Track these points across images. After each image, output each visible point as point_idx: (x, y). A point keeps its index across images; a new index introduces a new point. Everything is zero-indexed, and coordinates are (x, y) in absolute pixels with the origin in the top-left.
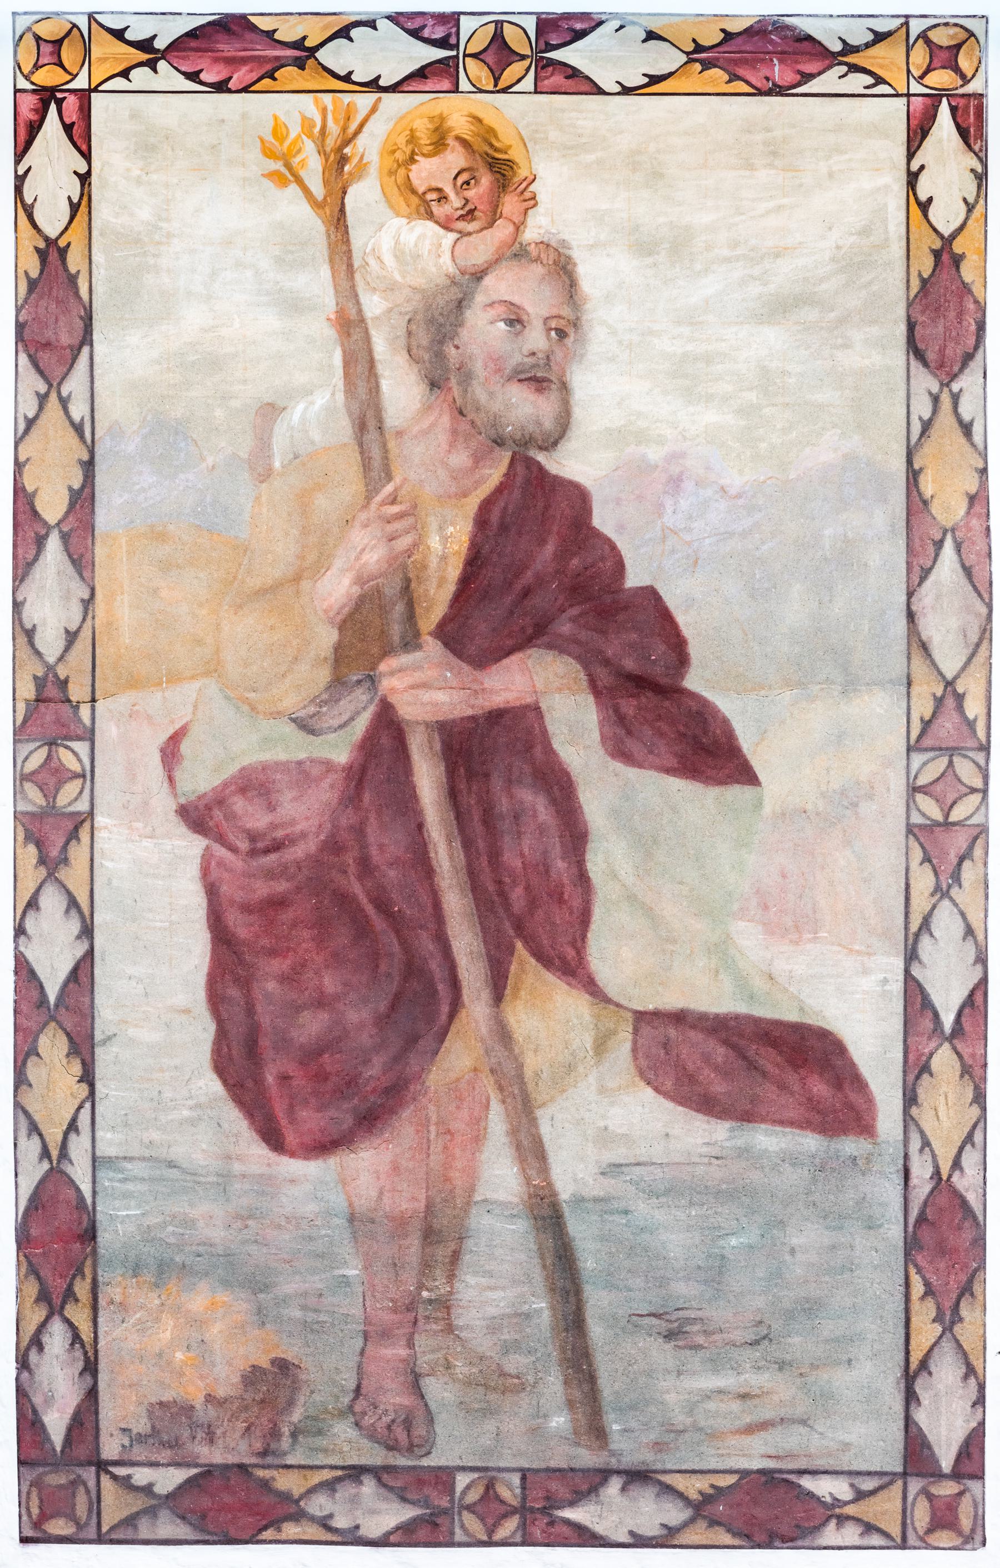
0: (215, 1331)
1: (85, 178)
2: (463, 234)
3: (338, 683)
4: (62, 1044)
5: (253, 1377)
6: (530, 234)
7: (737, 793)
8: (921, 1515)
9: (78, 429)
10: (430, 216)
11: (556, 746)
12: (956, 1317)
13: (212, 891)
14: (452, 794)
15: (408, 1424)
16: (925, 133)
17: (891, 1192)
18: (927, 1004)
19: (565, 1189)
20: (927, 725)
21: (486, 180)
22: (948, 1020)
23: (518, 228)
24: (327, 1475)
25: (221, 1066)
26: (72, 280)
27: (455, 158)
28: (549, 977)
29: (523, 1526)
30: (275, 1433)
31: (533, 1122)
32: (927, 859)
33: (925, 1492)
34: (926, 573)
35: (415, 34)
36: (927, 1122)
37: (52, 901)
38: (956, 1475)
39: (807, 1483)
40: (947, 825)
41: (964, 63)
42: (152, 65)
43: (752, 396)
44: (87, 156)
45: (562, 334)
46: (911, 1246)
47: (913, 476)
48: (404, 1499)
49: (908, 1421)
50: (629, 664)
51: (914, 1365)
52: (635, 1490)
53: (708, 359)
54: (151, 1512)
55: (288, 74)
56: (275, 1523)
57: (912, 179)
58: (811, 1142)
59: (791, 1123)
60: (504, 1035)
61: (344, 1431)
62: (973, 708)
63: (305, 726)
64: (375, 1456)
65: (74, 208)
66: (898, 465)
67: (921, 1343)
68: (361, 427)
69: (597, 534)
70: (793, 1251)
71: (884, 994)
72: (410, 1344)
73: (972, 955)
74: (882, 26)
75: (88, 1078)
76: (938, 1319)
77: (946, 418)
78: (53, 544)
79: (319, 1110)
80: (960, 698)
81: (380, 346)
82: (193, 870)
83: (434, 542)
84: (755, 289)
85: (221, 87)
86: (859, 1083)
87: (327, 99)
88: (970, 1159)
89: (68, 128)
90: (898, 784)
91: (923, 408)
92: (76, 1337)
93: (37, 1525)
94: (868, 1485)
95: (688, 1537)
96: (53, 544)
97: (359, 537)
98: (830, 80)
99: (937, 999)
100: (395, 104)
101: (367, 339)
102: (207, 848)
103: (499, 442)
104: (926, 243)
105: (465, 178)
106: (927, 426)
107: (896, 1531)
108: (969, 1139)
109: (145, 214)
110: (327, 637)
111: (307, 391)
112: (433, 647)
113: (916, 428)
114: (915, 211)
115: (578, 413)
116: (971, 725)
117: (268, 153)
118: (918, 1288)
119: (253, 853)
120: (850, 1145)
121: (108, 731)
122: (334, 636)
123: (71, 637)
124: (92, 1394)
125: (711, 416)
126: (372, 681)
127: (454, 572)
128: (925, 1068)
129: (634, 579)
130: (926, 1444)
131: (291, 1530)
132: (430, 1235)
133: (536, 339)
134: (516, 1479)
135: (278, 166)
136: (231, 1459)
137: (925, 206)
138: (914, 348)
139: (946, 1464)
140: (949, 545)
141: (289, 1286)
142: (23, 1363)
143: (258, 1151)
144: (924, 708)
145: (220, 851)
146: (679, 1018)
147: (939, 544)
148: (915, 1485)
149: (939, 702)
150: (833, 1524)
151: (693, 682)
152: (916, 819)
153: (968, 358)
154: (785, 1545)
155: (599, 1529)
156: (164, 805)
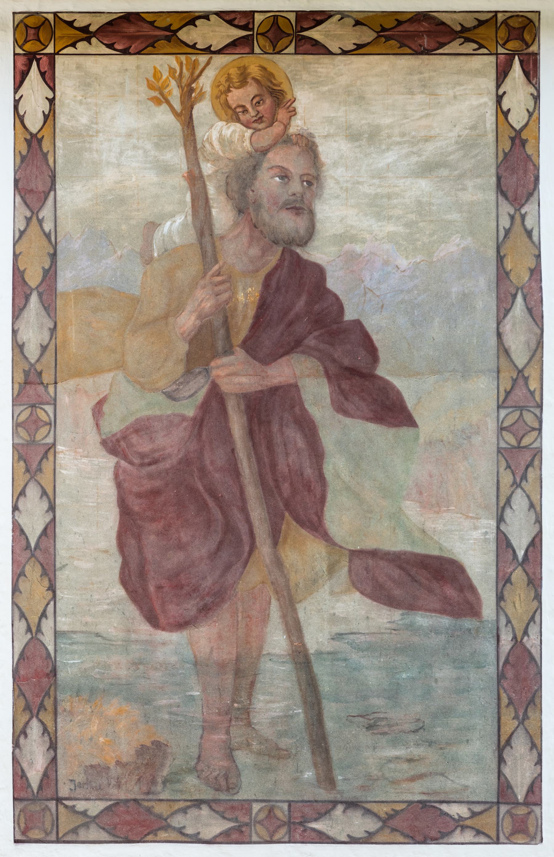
1: (52, 101)
2: (256, 130)
4: (38, 570)
5: (142, 750)
7: (405, 432)
8: (507, 826)
9: (48, 236)
10: (238, 120)
12: (526, 716)
13: (119, 485)
14: (251, 433)
18: (509, 545)
19: (312, 646)
20: (508, 393)
21: (268, 101)
22: (521, 554)
23: (286, 126)
24: (182, 805)
25: (124, 582)
27: (252, 89)
28: (303, 532)
30: (153, 781)
32: (509, 467)
34: (508, 311)
35: (230, 22)
36: (510, 611)
37: (33, 491)
38: (526, 803)
39: (444, 807)
41: (527, 37)
43: (413, 217)
44: (53, 89)
45: (310, 183)
46: (501, 677)
47: (500, 259)
48: (224, 818)
50: (346, 362)
51: (503, 742)
52: (350, 813)
53: (389, 197)
54: (86, 825)
56: (154, 832)
57: (499, 99)
58: (445, 621)
59: (435, 611)
60: (279, 563)
62: (533, 385)
63: (170, 396)
64: (208, 794)
65: (46, 117)
66: (492, 253)
67: (507, 730)
68: (201, 234)
69: (329, 291)
71: (486, 540)
72: (228, 733)
74: (483, 17)
75: (52, 588)
76: (516, 717)
78: (34, 298)
80: (526, 379)
81: (211, 190)
82: (110, 475)
83: (241, 296)
84: (414, 159)
85: (125, 52)
86: (472, 588)
87: (183, 58)
88: (533, 630)
89: (43, 74)
90: (492, 425)
91: (505, 222)
92: (45, 730)
93: (24, 833)
94: (478, 808)
95: (378, 838)
96: (34, 298)
97: (200, 294)
98: (454, 47)
99: (515, 543)
100: (220, 60)
101: (205, 187)
102: (117, 467)
103: (276, 242)
104: (507, 133)
105: (257, 100)
106: (508, 232)
107: (493, 834)
108: (532, 619)
109: (84, 120)
111: (172, 215)
112: (240, 354)
113: (502, 233)
115: (318, 226)
116: (532, 393)
117: (151, 86)
118: (505, 700)
119: (142, 465)
120: (468, 623)
121: (64, 399)
123: (44, 348)
124: (54, 760)
125: (391, 228)
127: (251, 313)
128: (508, 581)
129: (349, 315)
131: (163, 835)
132: (238, 673)
133: (296, 186)
134: (285, 806)
135: (156, 94)
136: (131, 796)
137: (506, 114)
138: (500, 190)
139: (520, 797)
140: (519, 299)
142: (16, 744)
143: (145, 627)
144: (506, 384)
145: (123, 463)
146: (374, 554)
147: (515, 296)
148: (504, 809)
150: (458, 831)
151: (381, 371)
152: (503, 445)
153: (531, 195)
156: (93, 439)
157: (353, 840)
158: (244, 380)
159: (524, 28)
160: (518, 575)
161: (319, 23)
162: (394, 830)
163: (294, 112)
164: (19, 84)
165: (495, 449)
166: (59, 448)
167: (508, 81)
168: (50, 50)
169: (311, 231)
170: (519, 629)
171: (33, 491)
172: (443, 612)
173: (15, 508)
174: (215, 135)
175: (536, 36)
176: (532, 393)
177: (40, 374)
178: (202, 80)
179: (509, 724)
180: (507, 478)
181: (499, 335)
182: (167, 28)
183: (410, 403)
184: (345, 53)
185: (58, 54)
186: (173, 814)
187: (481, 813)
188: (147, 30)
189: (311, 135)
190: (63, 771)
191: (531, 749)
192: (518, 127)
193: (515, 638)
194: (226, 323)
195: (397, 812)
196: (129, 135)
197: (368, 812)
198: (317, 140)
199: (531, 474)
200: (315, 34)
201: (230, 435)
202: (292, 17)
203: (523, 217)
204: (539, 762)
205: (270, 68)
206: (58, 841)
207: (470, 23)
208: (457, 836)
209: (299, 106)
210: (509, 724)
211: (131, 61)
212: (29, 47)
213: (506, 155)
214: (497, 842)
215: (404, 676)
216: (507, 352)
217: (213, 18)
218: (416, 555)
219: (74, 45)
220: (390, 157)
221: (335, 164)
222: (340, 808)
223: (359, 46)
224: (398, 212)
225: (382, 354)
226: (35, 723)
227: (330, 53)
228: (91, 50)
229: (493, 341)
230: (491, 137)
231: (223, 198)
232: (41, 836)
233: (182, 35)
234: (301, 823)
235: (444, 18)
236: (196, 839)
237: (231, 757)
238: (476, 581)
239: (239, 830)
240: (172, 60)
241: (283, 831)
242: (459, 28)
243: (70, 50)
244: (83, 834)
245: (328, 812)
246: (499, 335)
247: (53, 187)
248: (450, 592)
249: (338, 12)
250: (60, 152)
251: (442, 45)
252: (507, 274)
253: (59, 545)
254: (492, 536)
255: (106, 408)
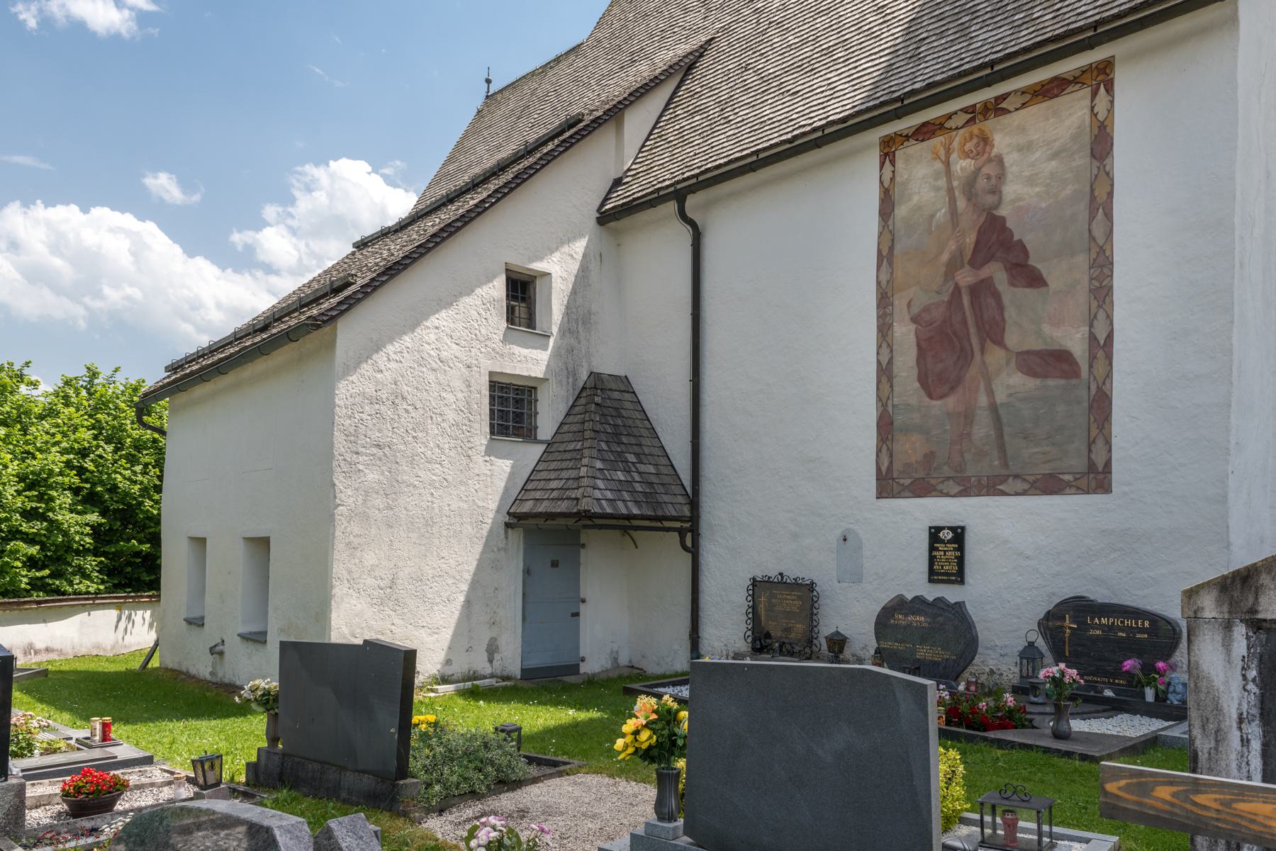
0: (918, 444)
1: (893, 172)
2: (976, 159)
3: (946, 281)
4: (886, 379)
5: (926, 456)
6: (993, 155)
7: (1043, 289)
8: (1093, 484)
9: (891, 232)
10: (969, 157)
11: (996, 286)
12: (1103, 427)
13: (917, 337)
14: (972, 303)
15: (960, 466)
16: (1096, 94)
17: (1084, 393)
18: (1096, 339)
19: (998, 401)
20: (1095, 260)
21: (982, 144)
22: (1102, 342)
23: (990, 154)
24: (942, 479)
25: (919, 380)
26: (891, 197)
27: (975, 141)
28: (995, 347)
29: (988, 491)
30: (930, 470)
31: (990, 385)
32: (1095, 298)
33: (1095, 478)
34: (1094, 218)
35: (966, 112)
36: (1095, 372)
37: (884, 345)
38: (1103, 472)
39: (1061, 476)
40: (1101, 287)
41: (1108, 71)
42: (908, 140)
43: (1048, 181)
44: (894, 166)
45: (1000, 178)
46: (1091, 407)
47: (1092, 190)
48: (959, 485)
49: (1089, 458)
50: (1014, 261)
51: (1091, 439)
52: (1015, 480)
53: (1037, 174)
54: (903, 490)
55: (938, 132)
56: (930, 492)
57: (1092, 108)
58: (1062, 382)
59: (1057, 377)
60: (984, 363)
61: (946, 468)
62: (1108, 253)
63: (938, 293)
64: (952, 474)
65: (891, 179)
66: (1088, 189)
67: (1093, 434)
68: (952, 215)
69: (1007, 228)
70: (1057, 412)
71: (1083, 338)
72: (961, 445)
73: (1109, 323)
74: (1084, 69)
75: (892, 386)
76: (1098, 428)
77: (1102, 172)
78: (885, 261)
79: (1218, 846)
80: (1104, 251)
81: (957, 193)
82: (913, 332)
83: (968, 240)
84: (1049, 152)
85: (923, 140)
86: (1076, 363)
87: (946, 135)
88: (1108, 382)
89: (890, 161)
90: (1086, 278)
91: (1095, 171)
92: (888, 449)
93: (880, 494)
94: (1078, 476)
95: (1029, 492)
96: (885, 261)
97: (951, 243)
98: (1071, 89)
99: (1098, 337)
100: (961, 131)
101: (954, 193)
102: (917, 328)
103: (983, 210)
104: (1096, 124)
105: (977, 145)
106: (1096, 176)
107: (1086, 489)
108: (1108, 376)
109: (906, 177)
110: (944, 269)
111: (940, 209)
112: (967, 267)
113: (1093, 177)
114: (1093, 117)
115: (1003, 198)
116: (1107, 258)
117: (933, 153)
118: (1092, 419)
119: (926, 326)
120: (1074, 381)
121: (896, 302)
122: (944, 269)
123: (888, 282)
124: (891, 462)
125: (1037, 189)
126: (954, 278)
127: (972, 246)
128: (1095, 357)
129: (1016, 238)
130: (1094, 464)
131: (933, 493)
132: (966, 417)
133: (993, 181)
134: (986, 478)
135: (934, 156)
136: (921, 476)
137: (1096, 115)
138: (1093, 155)
139: (1100, 469)
140: (1101, 210)
141: (934, 433)
142: (877, 456)
143: (927, 399)
144: (1094, 255)
145: (919, 327)
146: (1028, 352)
147: (1098, 209)
148: (1091, 476)
149: (1098, 253)
150: (1068, 488)
151: (1031, 262)
152: (1092, 287)
153: (1109, 153)
154: (905, 333)
155: (1007, 491)
156: (907, 318)
157: (1017, 494)
158: (969, 279)
159: (1106, 67)
160: (1100, 354)
161: (1005, 99)
162: (1036, 489)
163: (993, 146)
164: (881, 168)
165: (1088, 290)
166: (894, 324)
167: (1098, 98)
168: (893, 149)
169: (1000, 201)
170: (1100, 381)
171: (884, 345)
172: (1061, 377)
173: (878, 353)
174: (958, 167)
175: (1112, 70)
176: (1107, 258)
177: (887, 293)
178: (954, 143)
179: (1094, 432)
180: (1094, 304)
181: (1090, 231)
182: (940, 124)
183: (1045, 275)
184: (1017, 109)
185: (1084, 474)
186: (938, 484)
187: (1079, 479)
188: (933, 128)
189: (1001, 155)
190: (895, 466)
191: (1106, 444)
192: (1101, 119)
193: (1098, 387)
194: (961, 254)
195: (1038, 480)
196: (923, 178)
197: (1024, 480)
198: (1004, 156)
199: (1107, 300)
200: (1003, 105)
201: (963, 305)
202: (993, 101)
203: (1105, 166)
204: (1110, 451)
205: (983, 128)
206: (893, 497)
207: (1077, 74)
208: (1067, 490)
209: (996, 143)
210: (1094, 432)
211: (925, 143)
212: (885, 151)
213: (1096, 136)
214: (1088, 493)
215: (1041, 411)
216: (1094, 239)
217: (959, 113)
218: (1047, 350)
219: (902, 144)
220: (1038, 154)
221: (1012, 165)
222: (1011, 478)
223: (1023, 104)
224: (1040, 181)
225: (1031, 254)
226: (884, 446)
227: (1010, 112)
228: (910, 144)
229: (1086, 234)
230: (1088, 129)
231: (962, 195)
232: (886, 495)
233: (946, 125)
234: (993, 486)
235: (1065, 76)
236: (948, 495)
237: (962, 456)
238: (1078, 360)
239: (965, 490)
240: (942, 138)
241: (984, 491)
242: (1072, 79)
243: (901, 147)
244: (903, 494)
245: (1006, 480)
246: (1090, 231)
247: (893, 210)
248: (1065, 367)
249: (1012, 91)
250: (896, 193)
251: (1064, 90)
252: (1095, 198)
253: (894, 367)
254: (1087, 335)
255: (912, 303)
